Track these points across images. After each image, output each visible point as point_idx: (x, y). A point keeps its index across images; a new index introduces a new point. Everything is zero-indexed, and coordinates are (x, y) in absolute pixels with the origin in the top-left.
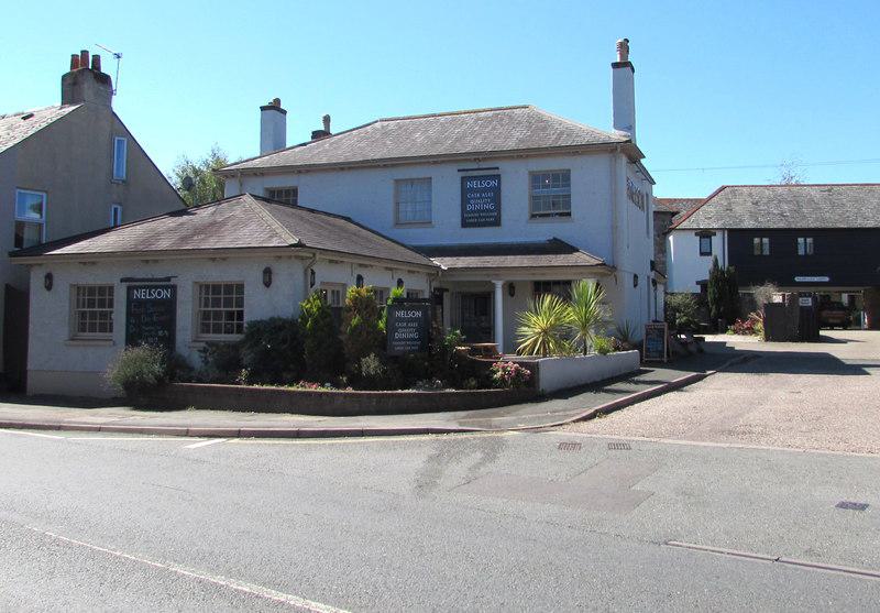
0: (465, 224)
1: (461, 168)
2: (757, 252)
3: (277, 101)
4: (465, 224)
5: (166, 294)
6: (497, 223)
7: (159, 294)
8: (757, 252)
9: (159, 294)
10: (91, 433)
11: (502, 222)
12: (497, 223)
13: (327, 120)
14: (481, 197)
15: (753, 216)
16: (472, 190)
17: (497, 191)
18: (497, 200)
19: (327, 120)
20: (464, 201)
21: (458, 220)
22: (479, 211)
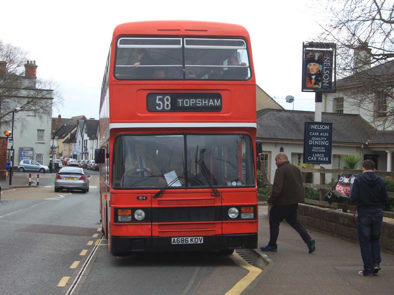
3: (287, 102)
7: (324, 127)
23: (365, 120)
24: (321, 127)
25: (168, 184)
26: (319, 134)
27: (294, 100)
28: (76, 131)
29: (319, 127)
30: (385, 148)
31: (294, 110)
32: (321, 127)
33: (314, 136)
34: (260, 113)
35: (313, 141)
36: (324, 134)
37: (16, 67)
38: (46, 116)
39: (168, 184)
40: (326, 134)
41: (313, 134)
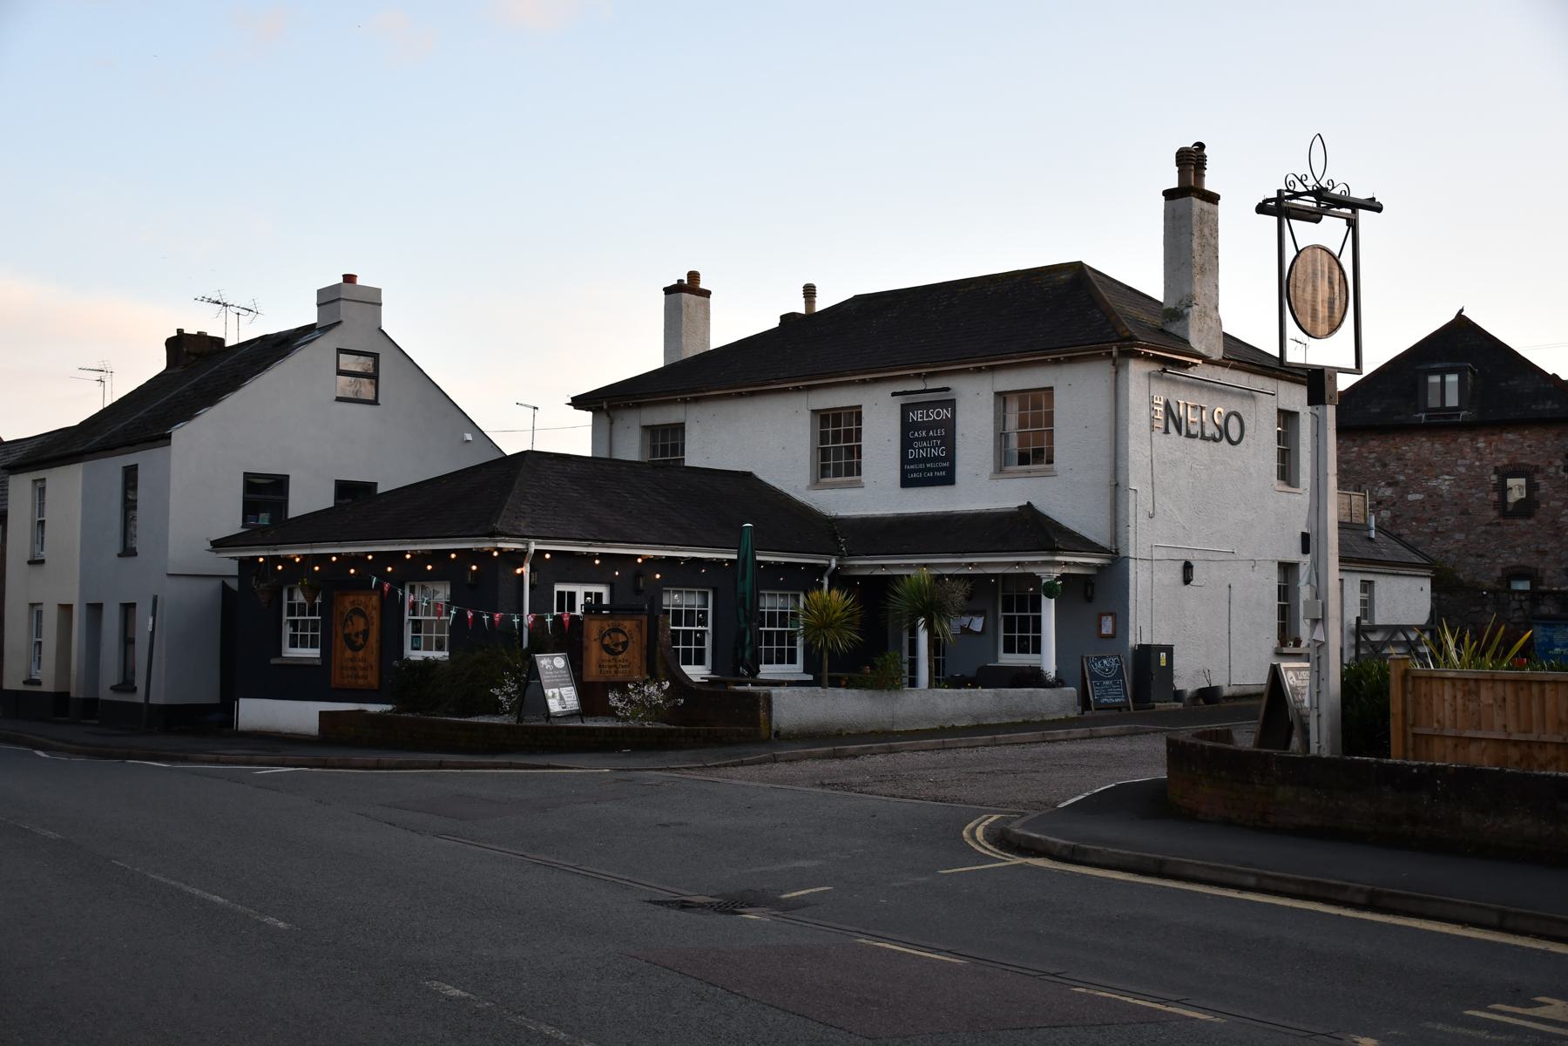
0: (907, 482)
1: (899, 389)
2: (1433, 402)
3: (693, 276)
4: (907, 482)
5: (945, 413)
6: (949, 479)
7: (938, 414)
8: (1433, 402)
9: (938, 414)
10: (1366, 574)
11: (958, 477)
12: (949, 479)
13: (809, 292)
14: (928, 438)
15: (817, 690)
16: (917, 426)
17: (950, 425)
18: (949, 442)
19: (809, 292)
20: (906, 443)
21: (896, 475)
22: (925, 460)
23: (930, 667)
24: (932, 413)
25: (1291, 221)
26: (927, 433)
27: (180, 331)
28: (1471, 646)
29: (928, 416)
30: (980, 845)
31: (535, 449)
32: (932, 413)
33: (917, 439)
34: (1336, 311)
35: (915, 449)
36: (937, 433)
37: (1318, 711)
38: (1106, 381)
39: (1291, 221)
40: (941, 432)
41: (916, 434)
